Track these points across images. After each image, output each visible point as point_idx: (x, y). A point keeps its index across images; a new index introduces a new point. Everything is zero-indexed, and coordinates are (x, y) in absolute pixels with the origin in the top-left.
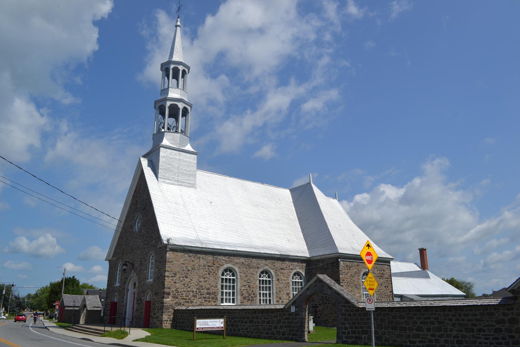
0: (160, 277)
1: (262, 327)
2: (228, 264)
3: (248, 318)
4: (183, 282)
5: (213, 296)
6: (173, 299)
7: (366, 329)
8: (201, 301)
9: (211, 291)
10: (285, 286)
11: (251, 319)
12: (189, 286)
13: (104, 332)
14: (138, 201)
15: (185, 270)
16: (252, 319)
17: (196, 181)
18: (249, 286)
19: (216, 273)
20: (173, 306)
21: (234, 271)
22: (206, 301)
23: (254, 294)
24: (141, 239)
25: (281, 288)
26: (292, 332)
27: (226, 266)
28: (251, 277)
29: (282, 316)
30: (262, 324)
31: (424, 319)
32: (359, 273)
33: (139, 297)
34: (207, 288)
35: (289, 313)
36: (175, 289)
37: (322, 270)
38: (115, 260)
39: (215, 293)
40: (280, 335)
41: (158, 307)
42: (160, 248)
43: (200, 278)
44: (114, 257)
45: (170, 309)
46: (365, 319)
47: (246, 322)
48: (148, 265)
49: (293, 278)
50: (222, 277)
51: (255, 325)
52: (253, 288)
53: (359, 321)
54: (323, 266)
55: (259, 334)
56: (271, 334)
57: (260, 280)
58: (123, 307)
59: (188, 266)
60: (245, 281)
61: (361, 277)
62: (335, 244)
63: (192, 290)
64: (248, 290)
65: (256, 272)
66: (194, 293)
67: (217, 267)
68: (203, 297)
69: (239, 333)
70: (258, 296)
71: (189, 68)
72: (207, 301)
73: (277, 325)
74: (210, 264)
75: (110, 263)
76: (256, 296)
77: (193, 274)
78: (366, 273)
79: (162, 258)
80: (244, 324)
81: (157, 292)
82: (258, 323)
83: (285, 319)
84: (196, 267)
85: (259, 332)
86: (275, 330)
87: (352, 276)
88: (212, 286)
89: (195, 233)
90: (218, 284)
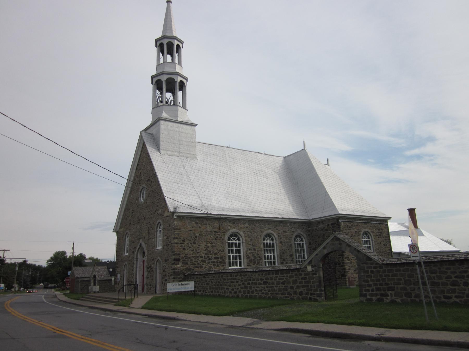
0: (169, 245)
1: (277, 288)
2: (234, 229)
3: (262, 279)
4: (191, 248)
5: (221, 260)
6: (183, 265)
7: (393, 286)
8: (209, 265)
9: (219, 255)
10: (288, 248)
11: (265, 280)
12: (198, 252)
13: (118, 301)
14: (141, 173)
15: (192, 236)
16: (266, 280)
17: (196, 152)
18: (254, 249)
19: (222, 238)
20: (183, 271)
21: (239, 236)
22: (214, 265)
23: (259, 257)
24: (147, 209)
25: (285, 250)
26: (310, 292)
27: (231, 231)
28: (256, 240)
29: (298, 276)
30: (277, 285)
31: (460, 273)
32: (358, 233)
33: (149, 265)
34: (214, 253)
35: (305, 272)
36: (185, 255)
37: (322, 231)
38: (122, 231)
39: (223, 257)
40: (297, 295)
41: (169, 273)
42: (167, 216)
43: (207, 244)
44: (122, 228)
45: (181, 275)
46: (391, 275)
47: (260, 284)
48: (156, 234)
49: (295, 240)
50: (229, 242)
51: (269, 286)
52: (259, 251)
53: (384, 277)
54: (324, 228)
55: (274, 295)
56: (288, 295)
57: (264, 243)
58: (134, 275)
59: (196, 233)
60: (250, 245)
61: (361, 236)
62: (335, 206)
63: (200, 255)
64: (254, 253)
65: (261, 236)
66: (202, 258)
67: (223, 233)
68: (212, 261)
69: (253, 295)
70: (264, 258)
71: (183, 42)
72: (215, 265)
73: (293, 285)
74: (216, 230)
75: (117, 234)
76: (262, 259)
77: (201, 240)
78: (366, 233)
79: (170, 226)
80: (258, 286)
81: (167, 259)
82: (273, 284)
83: (302, 279)
84: (203, 233)
85: (274, 293)
86: (291, 290)
87: (352, 236)
88: (219, 251)
89: (199, 200)
90: (225, 249)
